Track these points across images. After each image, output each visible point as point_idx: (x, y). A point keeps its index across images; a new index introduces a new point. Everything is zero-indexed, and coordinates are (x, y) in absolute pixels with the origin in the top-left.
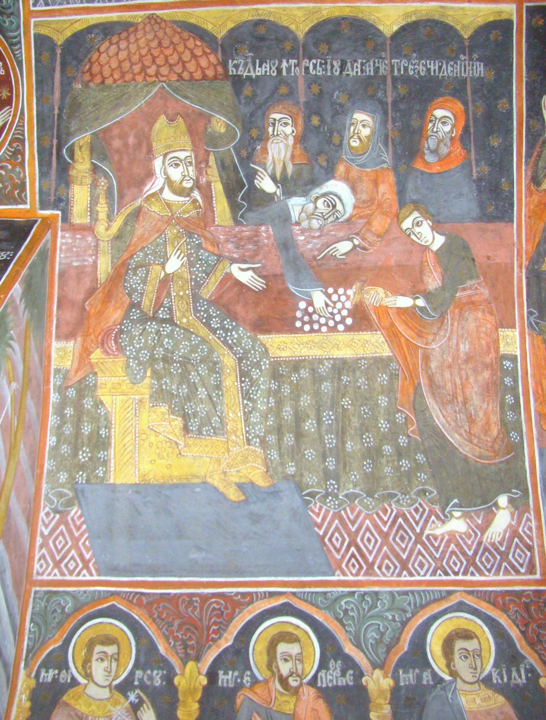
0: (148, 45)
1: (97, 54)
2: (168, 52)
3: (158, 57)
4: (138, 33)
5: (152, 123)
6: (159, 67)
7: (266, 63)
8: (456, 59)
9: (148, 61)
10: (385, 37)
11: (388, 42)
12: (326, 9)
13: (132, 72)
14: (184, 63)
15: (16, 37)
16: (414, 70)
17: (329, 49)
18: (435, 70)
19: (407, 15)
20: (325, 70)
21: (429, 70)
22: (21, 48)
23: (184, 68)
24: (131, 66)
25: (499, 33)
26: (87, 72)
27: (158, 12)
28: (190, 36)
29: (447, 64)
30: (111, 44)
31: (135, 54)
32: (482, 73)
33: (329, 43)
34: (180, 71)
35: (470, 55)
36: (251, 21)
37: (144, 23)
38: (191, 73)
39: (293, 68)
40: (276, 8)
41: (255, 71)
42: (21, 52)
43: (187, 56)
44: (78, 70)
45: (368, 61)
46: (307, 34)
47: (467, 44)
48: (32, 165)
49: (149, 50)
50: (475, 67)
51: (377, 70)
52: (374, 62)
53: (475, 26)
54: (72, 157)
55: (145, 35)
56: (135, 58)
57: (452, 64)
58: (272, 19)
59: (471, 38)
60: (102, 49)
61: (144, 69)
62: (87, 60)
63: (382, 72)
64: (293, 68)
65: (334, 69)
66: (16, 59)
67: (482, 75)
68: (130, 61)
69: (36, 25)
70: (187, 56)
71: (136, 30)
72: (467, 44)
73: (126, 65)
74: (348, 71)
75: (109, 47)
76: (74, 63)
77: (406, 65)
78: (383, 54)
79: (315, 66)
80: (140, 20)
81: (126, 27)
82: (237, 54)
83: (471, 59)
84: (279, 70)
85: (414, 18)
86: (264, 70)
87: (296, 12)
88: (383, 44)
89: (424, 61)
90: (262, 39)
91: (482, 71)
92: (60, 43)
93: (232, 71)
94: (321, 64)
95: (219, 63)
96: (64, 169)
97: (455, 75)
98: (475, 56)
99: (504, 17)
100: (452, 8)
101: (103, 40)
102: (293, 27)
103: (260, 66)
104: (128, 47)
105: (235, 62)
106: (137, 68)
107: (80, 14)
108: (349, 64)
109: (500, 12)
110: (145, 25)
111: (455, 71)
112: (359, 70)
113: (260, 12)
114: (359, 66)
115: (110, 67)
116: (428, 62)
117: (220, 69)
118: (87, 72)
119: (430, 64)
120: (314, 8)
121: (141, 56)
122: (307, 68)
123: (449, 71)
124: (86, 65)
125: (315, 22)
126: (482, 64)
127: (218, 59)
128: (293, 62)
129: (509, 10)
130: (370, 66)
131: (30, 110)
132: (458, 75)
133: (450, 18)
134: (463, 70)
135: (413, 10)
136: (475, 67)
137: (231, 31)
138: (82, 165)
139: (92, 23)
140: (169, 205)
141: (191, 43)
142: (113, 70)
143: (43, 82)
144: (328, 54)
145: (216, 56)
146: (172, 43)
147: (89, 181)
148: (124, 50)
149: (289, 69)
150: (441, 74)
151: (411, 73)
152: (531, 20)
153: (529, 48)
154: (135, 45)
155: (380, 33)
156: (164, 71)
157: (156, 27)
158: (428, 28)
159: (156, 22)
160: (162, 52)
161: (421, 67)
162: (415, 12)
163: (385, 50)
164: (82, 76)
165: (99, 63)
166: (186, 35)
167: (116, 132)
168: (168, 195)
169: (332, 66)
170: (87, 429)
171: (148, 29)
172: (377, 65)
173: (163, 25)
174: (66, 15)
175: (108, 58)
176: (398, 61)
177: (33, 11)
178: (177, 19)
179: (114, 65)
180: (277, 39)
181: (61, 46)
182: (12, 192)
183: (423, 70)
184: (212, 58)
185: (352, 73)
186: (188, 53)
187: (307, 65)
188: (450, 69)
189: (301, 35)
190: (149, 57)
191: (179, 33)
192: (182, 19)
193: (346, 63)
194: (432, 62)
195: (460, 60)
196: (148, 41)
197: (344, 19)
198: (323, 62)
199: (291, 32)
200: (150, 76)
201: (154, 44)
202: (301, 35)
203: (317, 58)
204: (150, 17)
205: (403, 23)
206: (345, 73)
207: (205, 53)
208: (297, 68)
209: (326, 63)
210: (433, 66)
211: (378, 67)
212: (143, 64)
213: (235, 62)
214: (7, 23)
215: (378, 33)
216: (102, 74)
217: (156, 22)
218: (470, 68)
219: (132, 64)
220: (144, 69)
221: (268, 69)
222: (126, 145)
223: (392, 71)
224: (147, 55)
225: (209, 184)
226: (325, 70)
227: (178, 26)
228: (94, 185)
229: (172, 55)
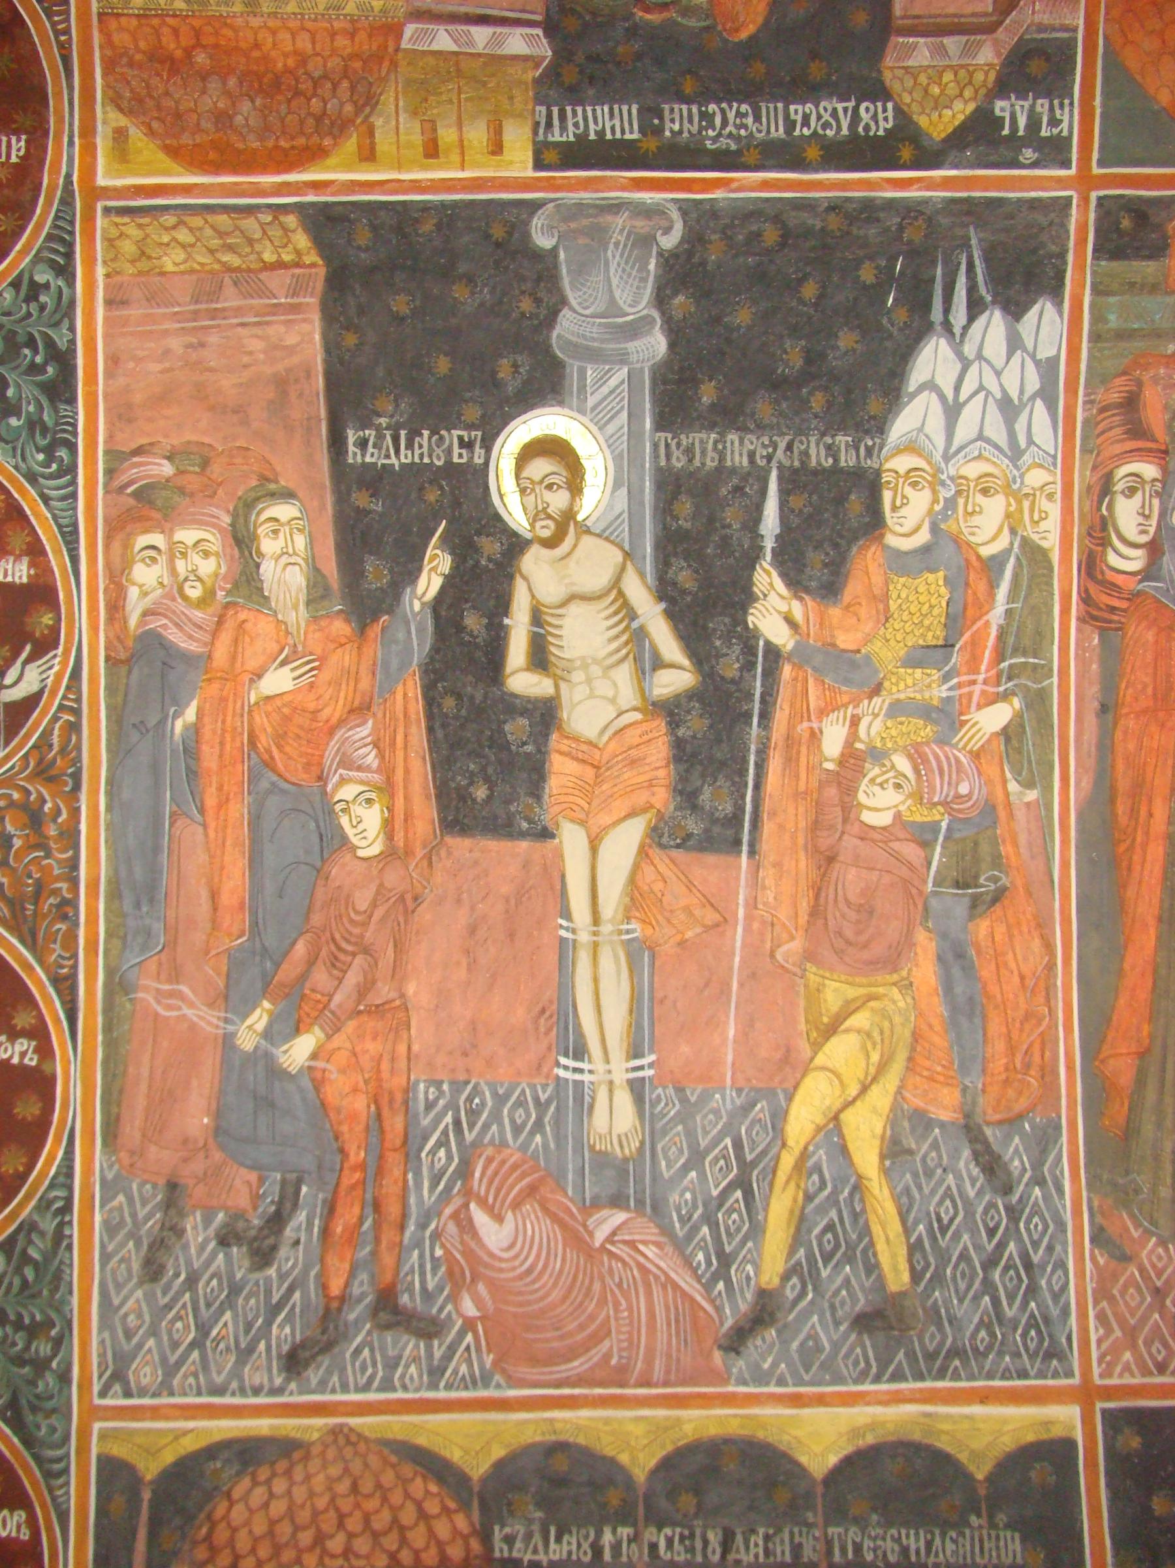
0: (330, 1489)
1: (225, 1504)
2: (371, 1505)
3: (350, 1514)
4: (310, 1463)
6: (351, 1536)
7: (570, 1532)
8: (961, 1523)
9: (328, 1523)
10: (813, 1480)
11: (820, 1490)
12: (690, 1421)
13: (296, 1546)
14: (402, 1529)
15: (59, 1460)
16: (875, 1550)
17: (699, 1506)
18: (918, 1552)
19: (855, 1432)
20: (691, 1550)
21: (905, 1550)
22: (67, 1483)
23: (403, 1541)
24: (294, 1534)
25: (1050, 1468)
26: (205, 1540)
27: (354, 1421)
28: (416, 1473)
29: (943, 1535)
30: (255, 1483)
31: (303, 1506)
32: (1019, 1556)
33: (697, 1492)
34: (394, 1547)
35: (991, 1516)
36: (540, 1444)
37: (323, 1443)
38: (417, 1553)
39: (625, 1545)
40: (590, 1419)
41: (546, 1552)
42: (68, 1493)
43: (408, 1516)
44: (183, 1537)
45: (779, 1530)
46: (654, 1472)
47: (982, 1492)
49: (333, 1500)
50: (1002, 1543)
51: (797, 1549)
52: (792, 1534)
53: (996, 1453)
55: (324, 1467)
56: (304, 1516)
57: (954, 1534)
58: (581, 1440)
59: (989, 1479)
60: (237, 1494)
61: (320, 1539)
62: (202, 1516)
63: (808, 1554)
64: (625, 1545)
65: (710, 1549)
66: (57, 1507)
67: (1019, 1560)
68: (293, 1521)
69: (103, 1436)
70: (408, 1516)
71: (307, 1457)
72: (982, 1492)
74: (738, 1551)
75: (250, 1490)
76: (177, 1521)
77: (858, 1540)
78: (810, 1517)
79: (670, 1542)
80: (316, 1436)
81: (287, 1449)
82: (512, 1513)
83: (993, 1525)
84: (597, 1551)
85: (870, 1439)
86: (565, 1548)
87: (631, 1427)
88: (809, 1495)
89: (894, 1531)
90: (560, 1482)
91: (1018, 1549)
92: (149, 1477)
93: (501, 1550)
94: (682, 1538)
95: (474, 1532)
97: (961, 1560)
98: (1001, 1518)
99: (1057, 1432)
100: (948, 1417)
101: (239, 1474)
102: (624, 1458)
103: (559, 1539)
104: (289, 1492)
105: (507, 1530)
106: (306, 1538)
107: (193, 1418)
108: (739, 1538)
109: (1047, 1424)
110: (326, 1446)
111: (961, 1551)
112: (761, 1551)
113: (558, 1426)
114: (761, 1543)
115: (250, 1532)
116: (903, 1532)
117: (476, 1545)
119: (908, 1536)
120: (667, 1418)
121: (316, 1514)
122: (654, 1547)
123: (948, 1553)
124: (200, 1527)
125: (670, 1448)
126: (1017, 1535)
127: (472, 1524)
128: (625, 1531)
129: (1066, 1418)
130: (782, 1541)
132: (969, 1560)
133: (944, 1438)
134: (977, 1549)
135: (869, 1420)
136: (1002, 1543)
137: (500, 1464)
139: (217, 1437)
141: (418, 1487)
142: (256, 1540)
144: (696, 1515)
145: (468, 1517)
146: (379, 1486)
148: (282, 1497)
149: (616, 1548)
150: (932, 1559)
151: (869, 1557)
152: (1114, 1438)
153: (1114, 1497)
154: (304, 1488)
155: (800, 1471)
156: (362, 1545)
157: (348, 1452)
158: (900, 1460)
159: (349, 1442)
160: (357, 1506)
161: (889, 1543)
162: (872, 1427)
163: (813, 1508)
164: (191, 1550)
165: (229, 1524)
166: (408, 1470)
169: (706, 1542)
171: (331, 1453)
172: (797, 1539)
173: (362, 1447)
174: (167, 1418)
175: (247, 1514)
176: (841, 1530)
177: (99, 1407)
178: (390, 1436)
179: (260, 1528)
180: (591, 1483)
181: (151, 1482)
183: (893, 1551)
184: (461, 1522)
185: (747, 1558)
186: (410, 1507)
187: (654, 1539)
188: (950, 1547)
189: (640, 1475)
190: (332, 1514)
191: (393, 1466)
192: (400, 1437)
193: (734, 1534)
194: (912, 1532)
195: (970, 1526)
196: (331, 1481)
197: (728, 1441)
198: (686, 1532)
199: (620, 1468)
200: (333, 1556)
201: (343, 1487)
202: (640, 1475)
203: (674, 1524)
204: (335, 1431)
205: (849, 1449)
206: (731, 1557)
207: (446, 1510)
208: (633, 1545)
209: (692, 1536)
210: (915, 1541)
211: (800, 1545)
212: (319, 1530)
213: (507, 1530)
214: (44, 1430)
215: (798, 1471)
216: (233, 1548)
217: (349, 1442)
218: (993, 1545)
219: (297, 1528)
220: (320, 1539)
221: (574, 1547)
223: (829, 1552)
224: (326, 1510)
226: (691, 1550)
227: (392, 1451)
229: (377, 1512)
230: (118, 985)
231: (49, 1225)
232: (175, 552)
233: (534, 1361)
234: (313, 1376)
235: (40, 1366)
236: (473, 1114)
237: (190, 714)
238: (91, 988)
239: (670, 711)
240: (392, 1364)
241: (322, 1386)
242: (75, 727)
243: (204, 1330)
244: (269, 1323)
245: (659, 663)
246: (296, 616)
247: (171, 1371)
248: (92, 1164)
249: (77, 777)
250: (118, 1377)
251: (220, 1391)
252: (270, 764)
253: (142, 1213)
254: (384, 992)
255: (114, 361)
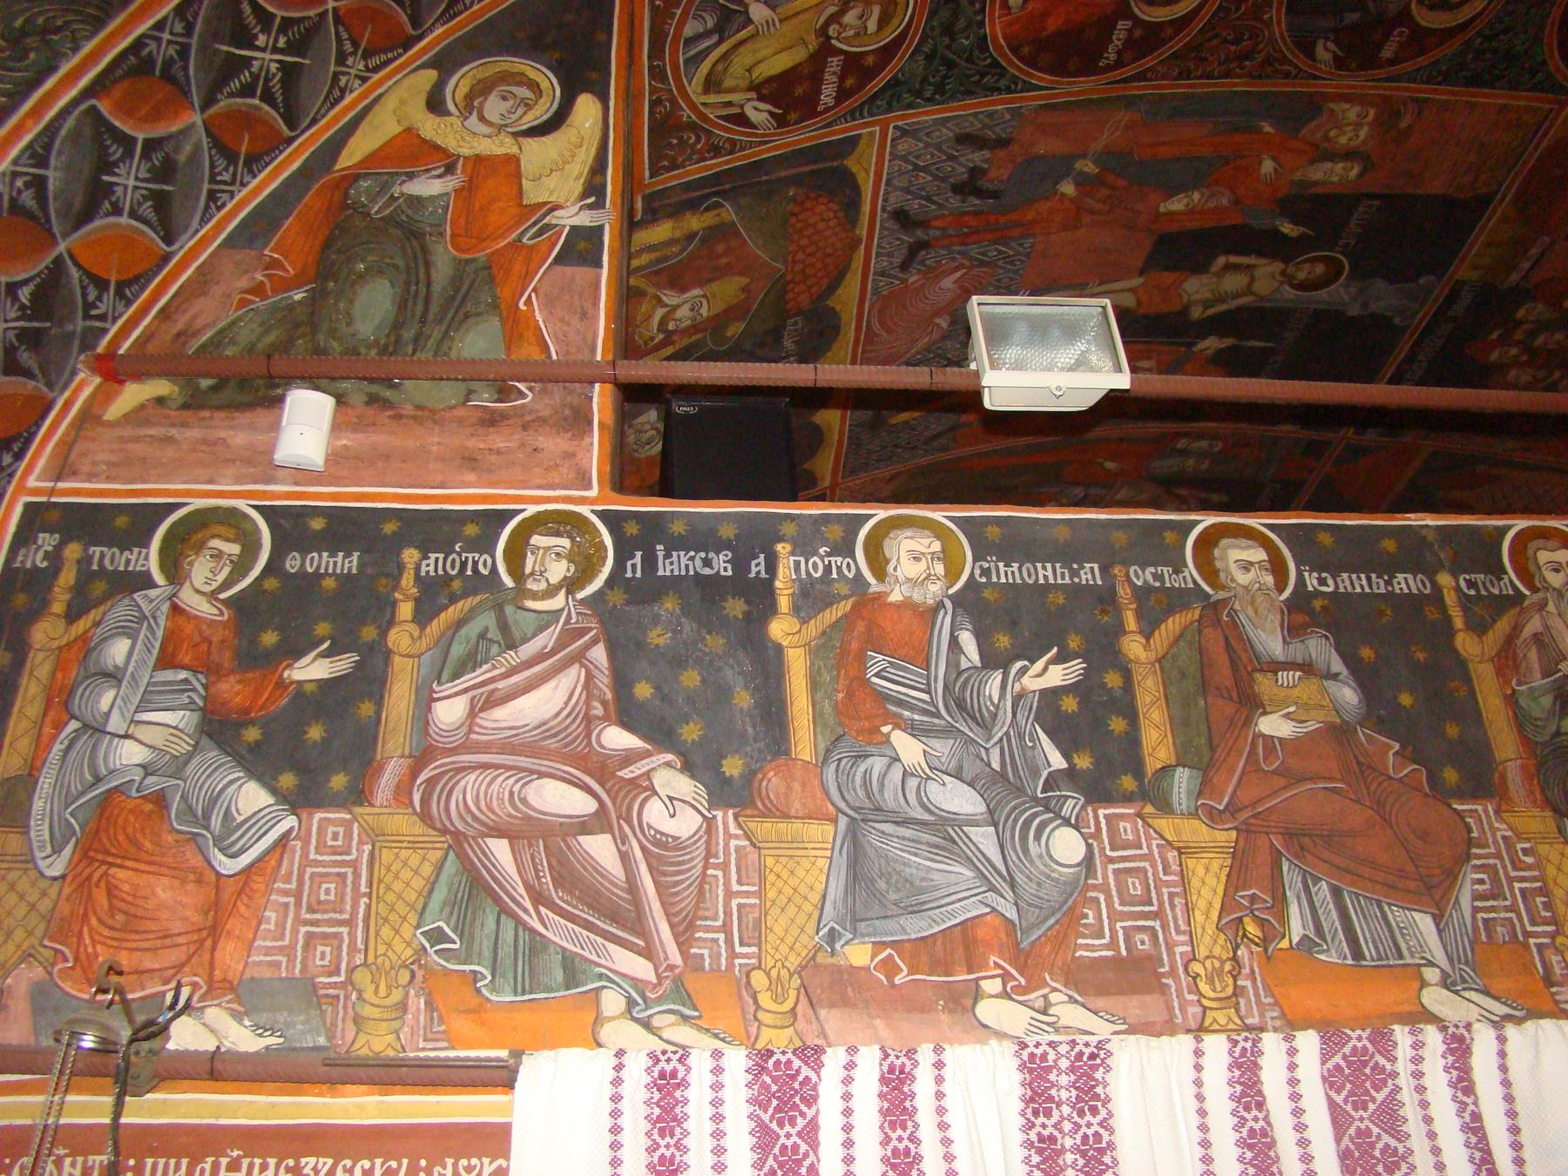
5: (742, 273)
48: (699, 170)
54: (707, 209)
61: (803, 248)
73: (810, 231)
96: (693, 206)
118: (1252, 294)
131: (769, 150)
138: (696, 222)
140: (649, 317)
143: (799, 156)
147: (678, 234)
156: (798, 267)
167: (734, 243)
168: (660, 312)
170: (1499, 27)
182: (666, 157)
189: (829, 303)
202: (829, 303)
222: (719, 257)
225: (672, 343)
228: (671, 242)
230: (1129, 102)
231: (1003, 83)
232: (1358, 125)
233: (880, 312)
234: (890, 224)
235: (919, 94)
236: (1012, 263)
237: (1268, 129)
238: (1134, 90)
239: (1185, 311)
240: (890, 255)
241: (883, 228)
242: (1287, 75)
243: (924, 169)
244: (922, 198)
245: (1206, 308)
246: (1298, 176)
247: (905, 159)
248: (1031, 101)
249: (1260, 77)
250: (904, 132)
251: (887, 184)
252: (1227, 163)
253: (997, 129)
254: (1086, 219)
255: (1472, 106)
